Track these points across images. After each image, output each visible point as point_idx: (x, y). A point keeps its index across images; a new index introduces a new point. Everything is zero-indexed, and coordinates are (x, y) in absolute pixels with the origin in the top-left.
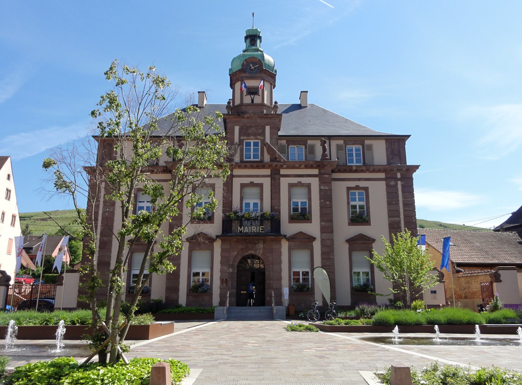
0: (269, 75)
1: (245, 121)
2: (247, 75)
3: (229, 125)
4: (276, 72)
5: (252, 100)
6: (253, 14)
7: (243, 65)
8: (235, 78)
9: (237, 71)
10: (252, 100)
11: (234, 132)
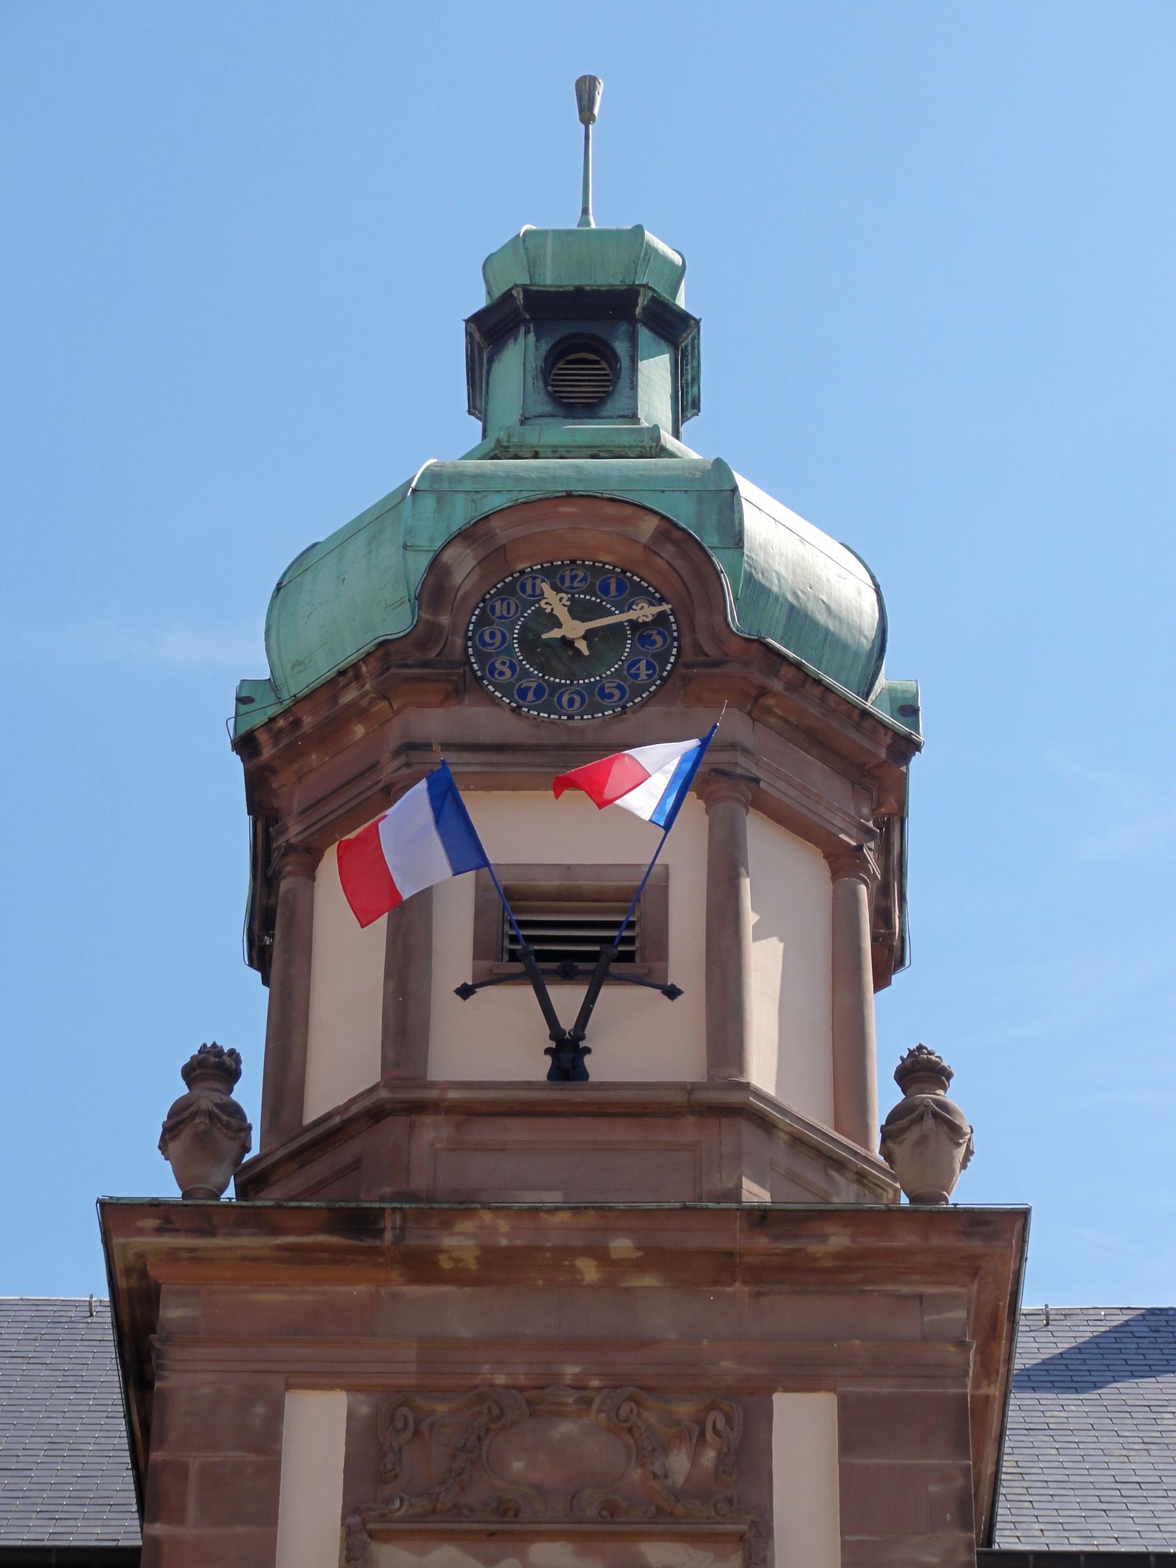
0: (815, 740)
1: (459, 1314)
2: (484, 719)
3: (186, 1380)
4: (909, 711)
5: (567, 1054)
6: (585, 90)
7: (435, 589)
8: (308, 774)
9: (349, 673)
10: (567, 1054)
11: (271, 1470)
